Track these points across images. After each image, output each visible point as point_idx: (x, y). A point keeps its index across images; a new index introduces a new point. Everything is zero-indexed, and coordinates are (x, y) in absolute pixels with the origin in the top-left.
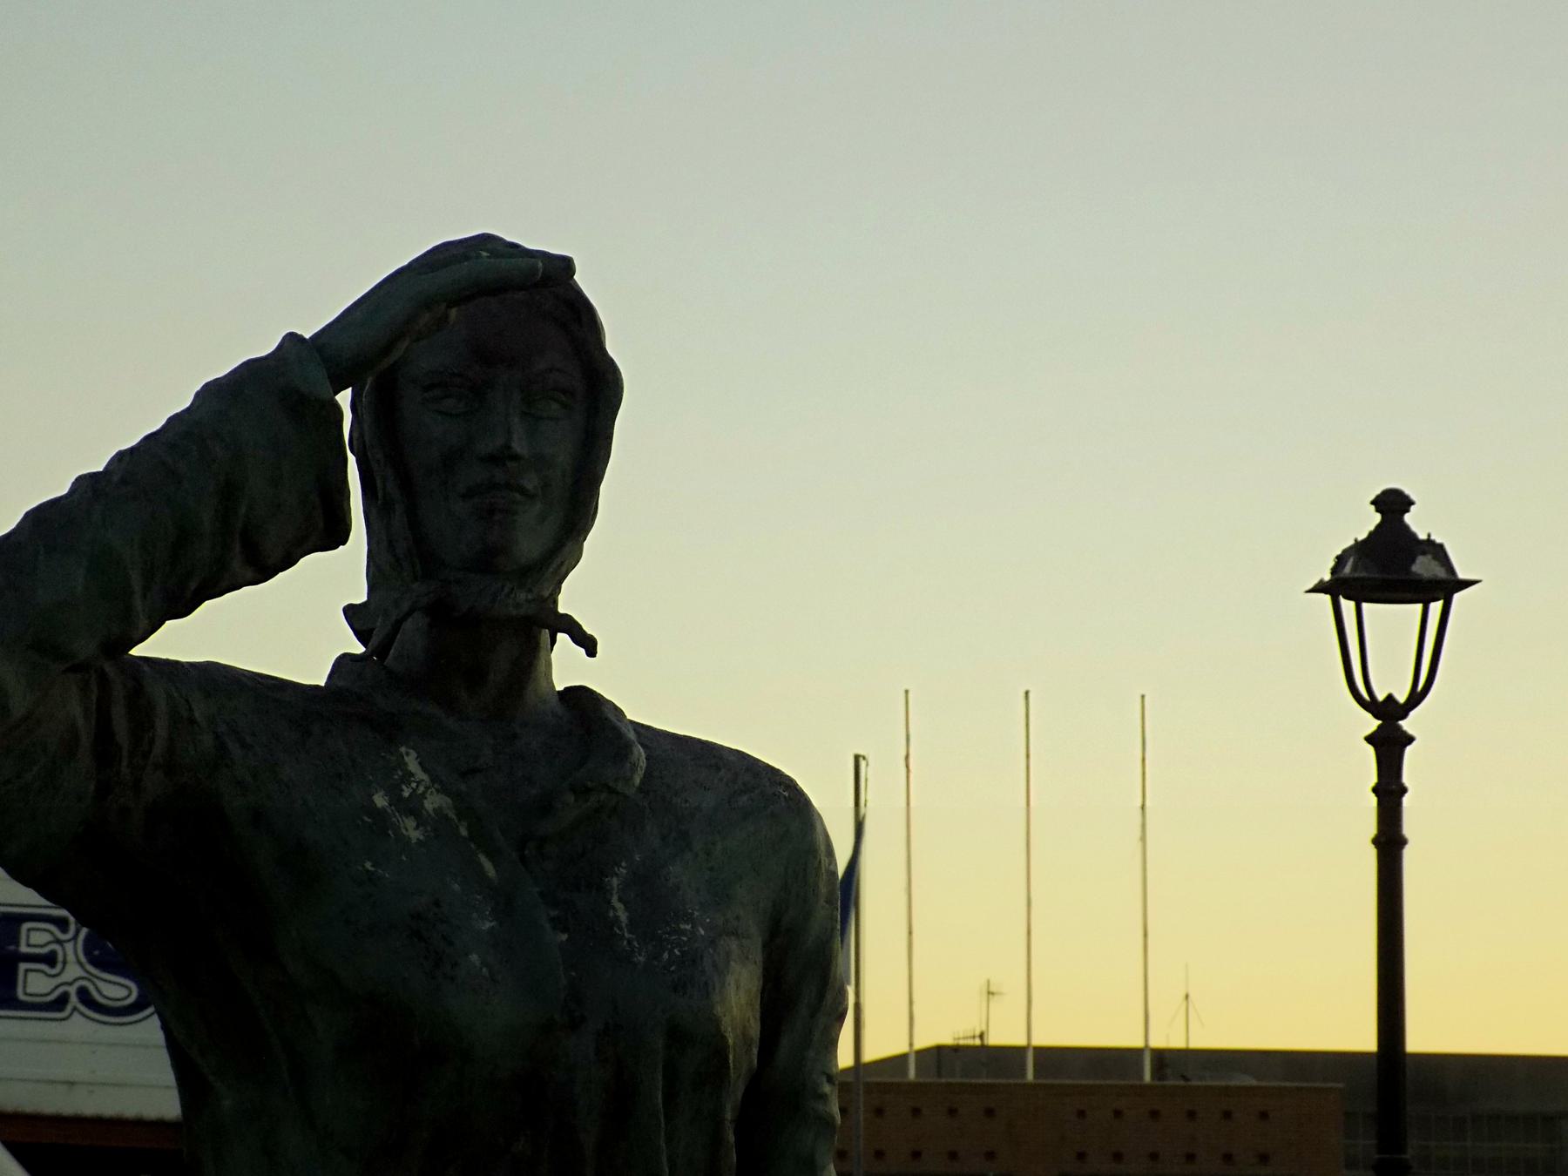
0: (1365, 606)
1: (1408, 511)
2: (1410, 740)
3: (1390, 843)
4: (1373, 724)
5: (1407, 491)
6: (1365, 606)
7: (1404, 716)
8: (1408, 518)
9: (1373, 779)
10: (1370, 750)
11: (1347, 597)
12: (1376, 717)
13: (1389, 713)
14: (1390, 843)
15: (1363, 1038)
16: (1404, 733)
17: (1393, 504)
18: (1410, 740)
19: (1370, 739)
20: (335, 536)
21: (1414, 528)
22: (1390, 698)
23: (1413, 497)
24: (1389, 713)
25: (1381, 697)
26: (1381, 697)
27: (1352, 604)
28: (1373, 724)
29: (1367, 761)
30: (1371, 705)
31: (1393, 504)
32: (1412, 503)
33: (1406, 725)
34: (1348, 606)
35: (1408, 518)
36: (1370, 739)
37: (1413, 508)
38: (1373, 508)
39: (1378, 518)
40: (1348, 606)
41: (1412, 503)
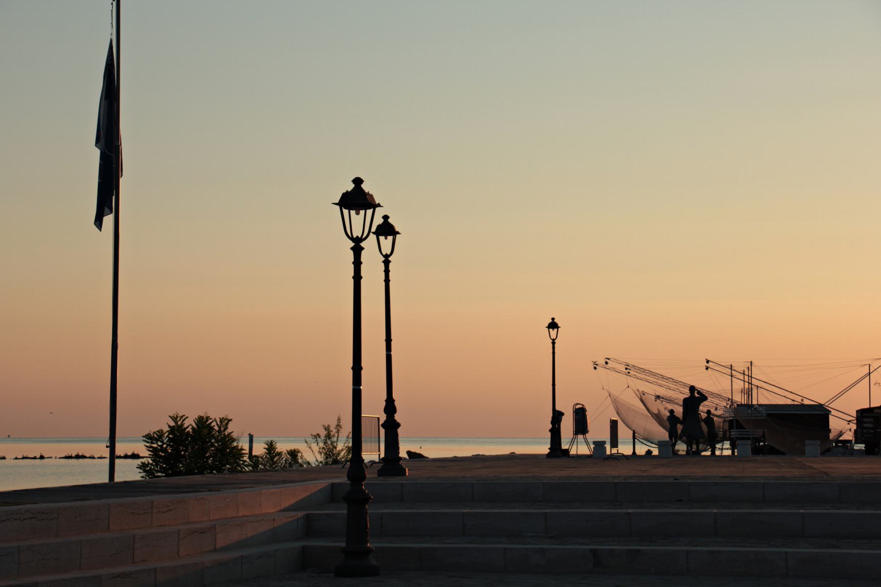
0: (351, 211)
1: (362, 183)
2: (363, 249)
3: (387, 281)
4: (352, 244)
5: (389, 215)
6: (351, 211)
7: (389, 257)
8: (362, 186)
9: (353, 260)
10: (383, 264)
11: (345, 208)
12: (353, 242)
13: (387, 257)
14: (387, 281)
15: (105, 479)
16: (362, 247)
17: (358, 181)
18: (363, 249)
19: (352, 249)
20: (112, 213)
21: (364, 188)
22: (357, 237)
23: (364, 180)
24: (387, 257)
25: (355, 236)
26: (355, 236)
27: (347, 211)
28: (352, 244)
29: (382, 266)
30: (351, 238)
31: (358, 181)
32: (363, 181)
33: (390, 259)
34: (346, 212)
35: (362, 186)
36: (352, 249)
37: (364, 183)
38: (352, 183)
39: (353, 185)
40: (346, 212)
41: (363, 181)
